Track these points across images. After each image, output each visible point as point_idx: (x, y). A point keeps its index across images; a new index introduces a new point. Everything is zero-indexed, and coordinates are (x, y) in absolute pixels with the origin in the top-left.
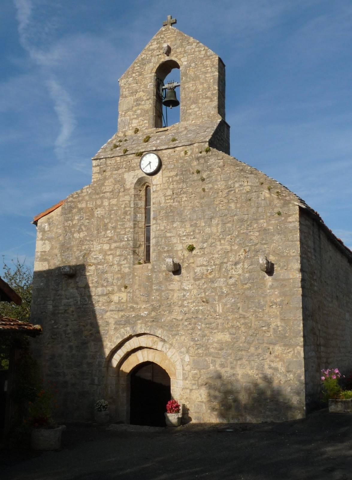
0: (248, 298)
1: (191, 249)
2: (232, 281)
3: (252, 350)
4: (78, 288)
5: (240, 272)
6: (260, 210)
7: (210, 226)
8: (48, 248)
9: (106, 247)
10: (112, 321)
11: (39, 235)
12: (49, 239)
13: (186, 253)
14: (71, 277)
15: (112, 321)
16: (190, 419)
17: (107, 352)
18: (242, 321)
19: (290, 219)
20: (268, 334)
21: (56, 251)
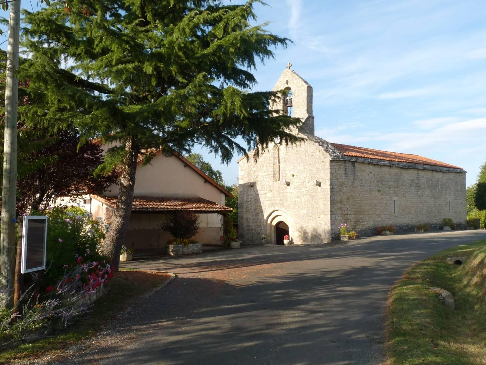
0: (312, 196)
1: (293, 176)
2: (307, 189)
3: (314, 216)
4: (254, 191)
5: (310, 185)
6: (316, 160)
7: (299, 166)
8: (243, 174)
9: (264, 174)
10: (267, 205)
11: (240, 169)
12: (243, 170)
13: (292, 177)
14: (252, 185)
15: (267, 205)
16: (294, 243)
17: (265, 217)
18: (311, 205)
19: (326, 164)
20: (319, 210)
21: (246, 175)
